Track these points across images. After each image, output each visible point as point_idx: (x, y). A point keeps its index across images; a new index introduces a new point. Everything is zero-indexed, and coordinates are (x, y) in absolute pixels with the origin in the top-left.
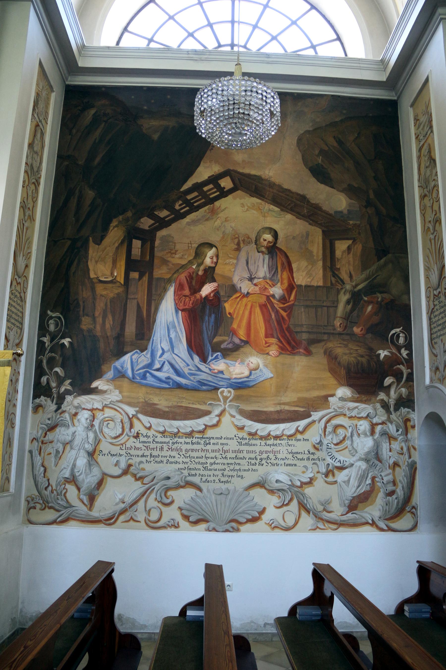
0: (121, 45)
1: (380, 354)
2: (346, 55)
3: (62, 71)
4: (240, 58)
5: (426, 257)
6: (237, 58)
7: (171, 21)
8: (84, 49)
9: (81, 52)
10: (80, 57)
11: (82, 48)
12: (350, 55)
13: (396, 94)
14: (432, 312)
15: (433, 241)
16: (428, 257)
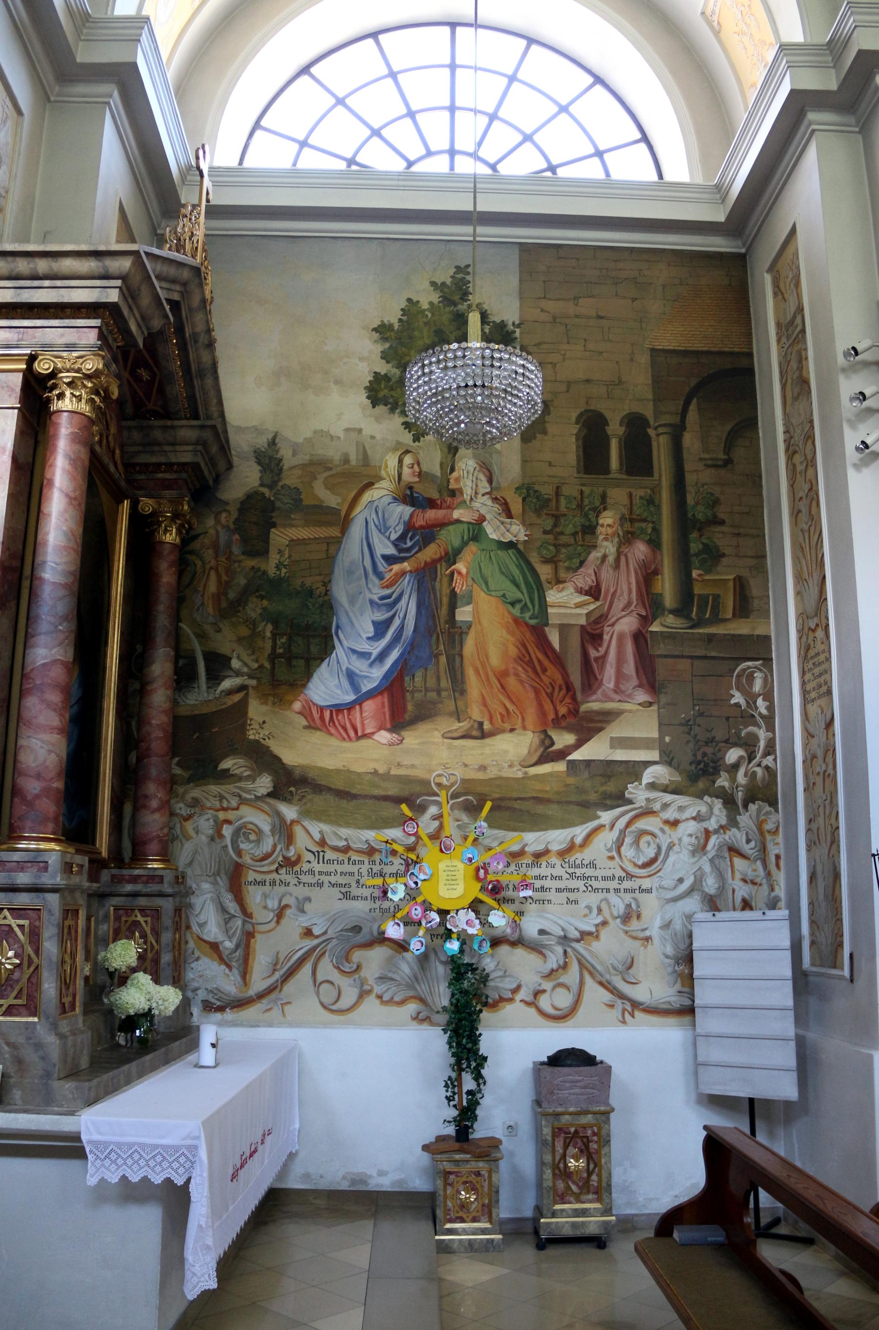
0: (246, 164)
1: (733, 696)
2: (661, 176)
3: (46, 84)
4: (478, 186)
5: (796, 559)
6: (472, 185)
7: (340, 108)
8: (87, 25)
9: (82, 32)
10: (81, 43)
11: (82, 19)
12: (669, 177)
13: (744, 245)
14: (808, 648)
15: (807, 535)
16: (798, 558)
